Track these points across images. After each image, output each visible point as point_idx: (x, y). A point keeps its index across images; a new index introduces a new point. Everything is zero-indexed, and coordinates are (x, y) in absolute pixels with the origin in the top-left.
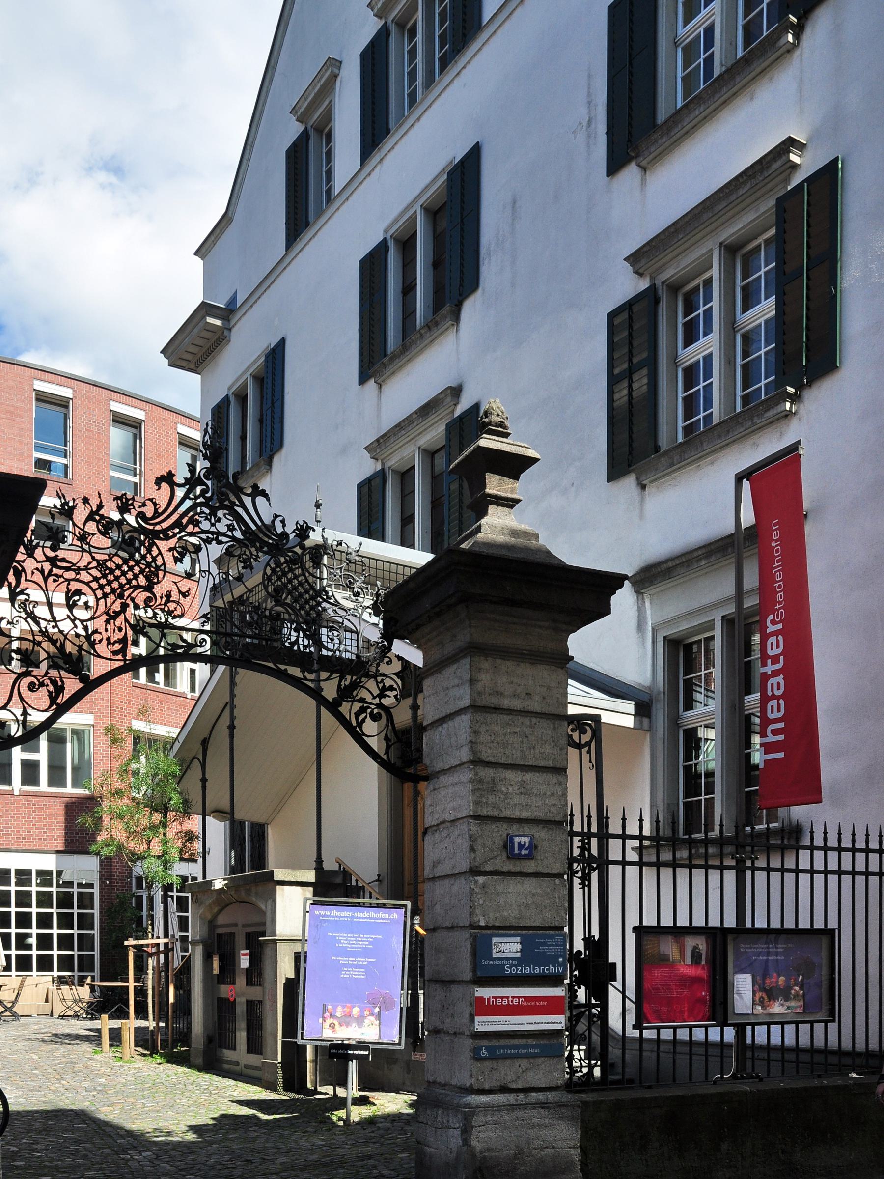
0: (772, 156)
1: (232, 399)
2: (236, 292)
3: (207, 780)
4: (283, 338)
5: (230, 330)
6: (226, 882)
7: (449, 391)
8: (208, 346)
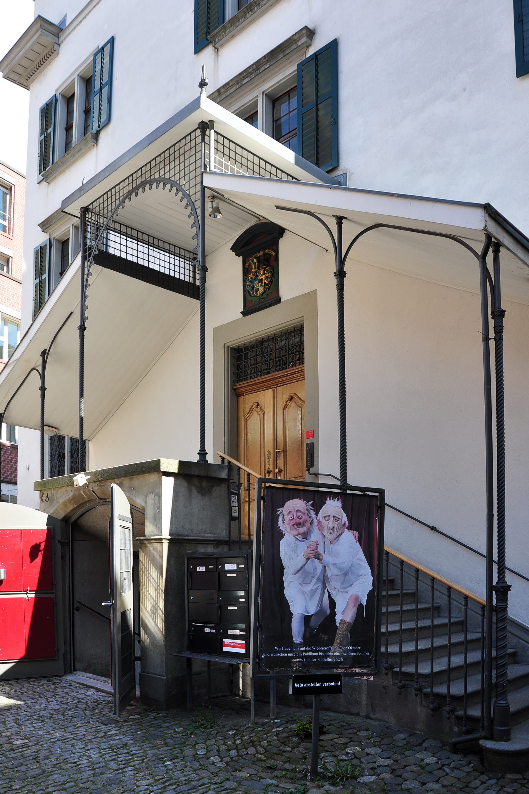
0: (325, 121)
1: (59, 98)
2: (66, 15)
3: (45, 389)
4: (113, 37)
5: (59, 45)
6: (89, 477)
7: (304, 32)
8: (38, 61)
